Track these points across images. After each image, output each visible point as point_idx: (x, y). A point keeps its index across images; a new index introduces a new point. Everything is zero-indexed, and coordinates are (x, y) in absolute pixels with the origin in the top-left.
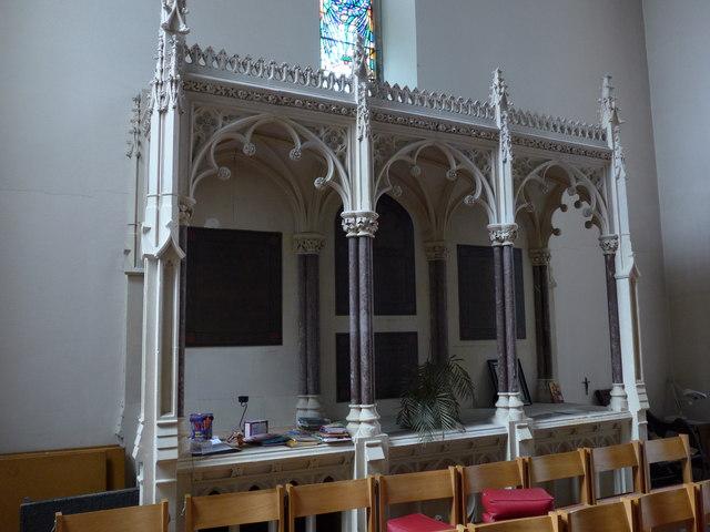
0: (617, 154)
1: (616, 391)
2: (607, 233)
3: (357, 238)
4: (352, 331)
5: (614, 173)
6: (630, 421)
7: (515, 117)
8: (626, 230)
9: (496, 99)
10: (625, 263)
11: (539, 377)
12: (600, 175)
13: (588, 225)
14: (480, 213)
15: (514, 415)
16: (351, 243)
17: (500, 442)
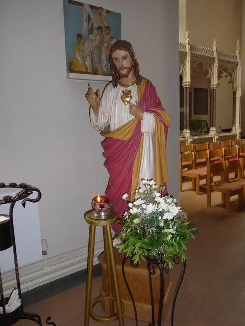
0: (239, 63)
1: (234, 128)
2: (235, 86)
3: (187, 88)
4: (185, 111)
5: (238, 68)
6: (237, 135)
7: (219, 54)
8: (240, 85)
9: (214, 49)
10: (239, 94)
11: (68, 73)
12: (234, 69)
13: (229, 83)
14: (209, 81)
15: (215, 132)
16: (185, 89)
17: (212, 138)
